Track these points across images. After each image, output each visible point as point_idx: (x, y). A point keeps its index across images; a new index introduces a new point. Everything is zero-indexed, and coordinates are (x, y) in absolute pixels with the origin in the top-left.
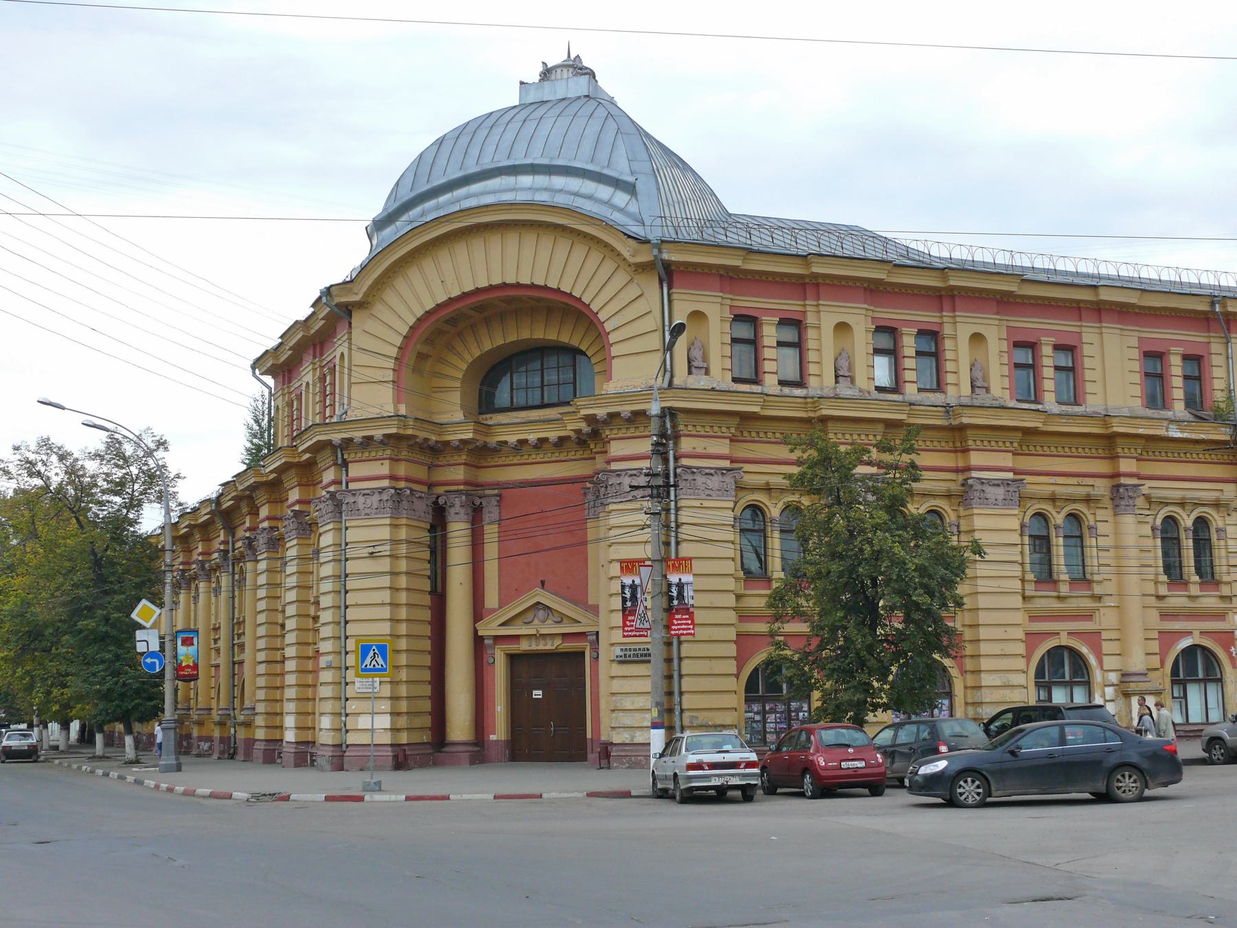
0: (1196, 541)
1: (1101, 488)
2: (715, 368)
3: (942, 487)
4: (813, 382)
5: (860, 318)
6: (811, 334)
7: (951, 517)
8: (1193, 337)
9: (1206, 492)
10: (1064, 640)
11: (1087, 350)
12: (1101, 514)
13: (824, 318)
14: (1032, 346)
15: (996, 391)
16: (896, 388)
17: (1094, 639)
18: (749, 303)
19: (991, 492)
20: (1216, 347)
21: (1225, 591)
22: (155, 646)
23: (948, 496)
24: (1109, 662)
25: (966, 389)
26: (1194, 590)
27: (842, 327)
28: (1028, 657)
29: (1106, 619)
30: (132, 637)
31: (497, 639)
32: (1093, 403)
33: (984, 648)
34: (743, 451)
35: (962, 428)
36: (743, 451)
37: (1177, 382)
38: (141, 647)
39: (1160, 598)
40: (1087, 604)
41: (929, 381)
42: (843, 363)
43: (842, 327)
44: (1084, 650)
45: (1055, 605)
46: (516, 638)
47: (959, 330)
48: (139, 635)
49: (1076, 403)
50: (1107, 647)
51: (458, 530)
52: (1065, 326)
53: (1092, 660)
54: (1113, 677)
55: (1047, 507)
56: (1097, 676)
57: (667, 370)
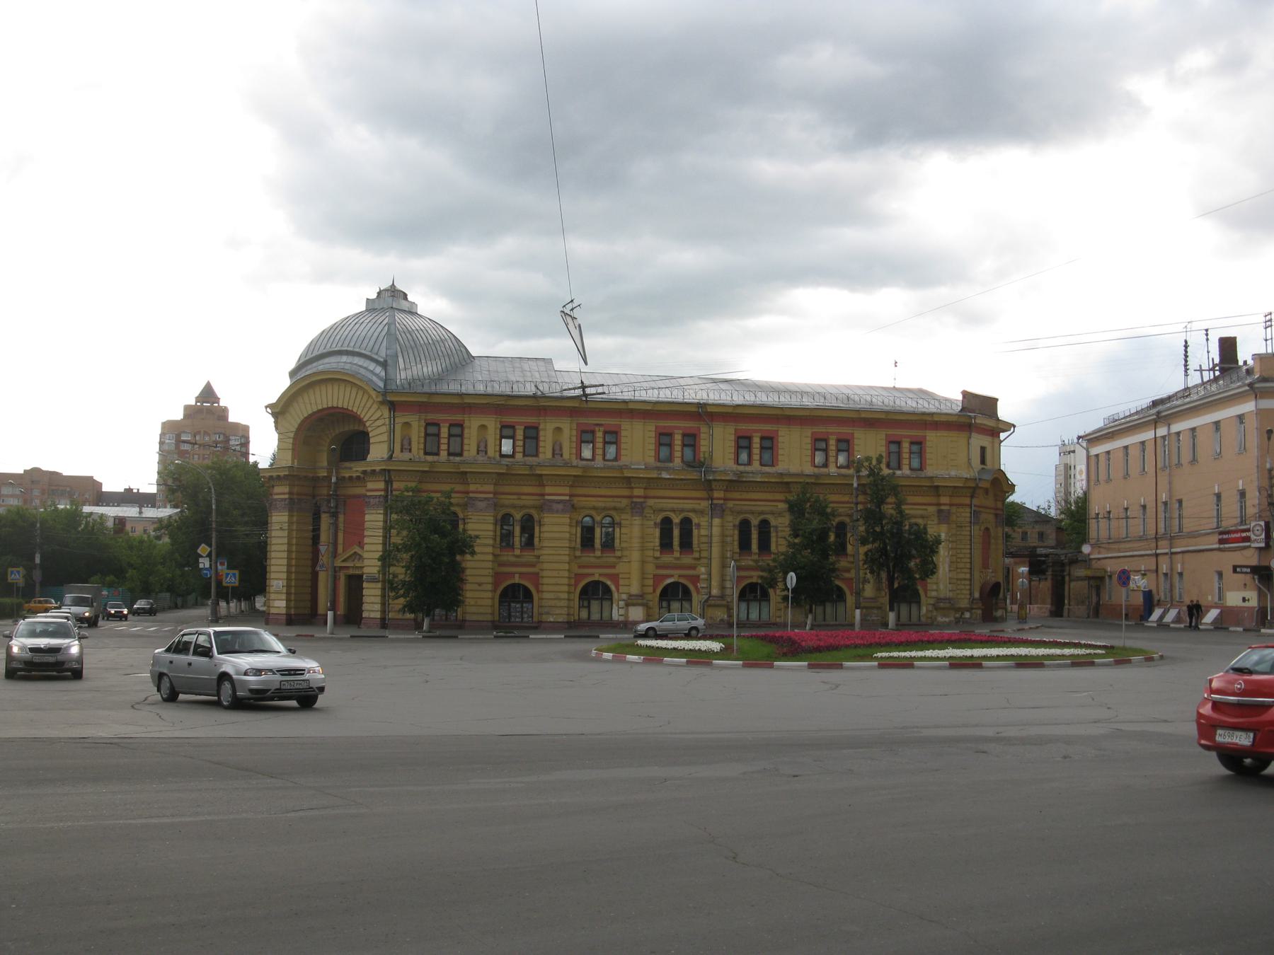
0: (760, 533)
1: (705, 504)
2: (414, 446)
3: (531, 503)
4: (465, 453)
5: (492, 424)
6: (466, 431)
7: (536, 517)
8: (689, 425)
9: (688, 505)
10: (517, 580)
11: (623, 433)
12: (623, 516)
13: (473, 425)
14: (899, 443)
15: (566, 456)
16: (593, 459)
17: (615, 578)
18: (432, 417)
19: (555, 506)
20: (704, 429)
21: (618, 554)
22: (207, 565)
23: (535, 507)
24: (622, 589)
25: (549, 455)
26: (517, 552)
27: (483, 427)
28: (576, 585)
29: (621, 568)
30: (198, 562)
31: (341, 568)
32: (930, 471)
33: (566, 581)
34: (729, 495)
35: (937, 487)
36: (729, 495)
37: (678, 448)
38: (201, 566)
39: (657, 558)
40: (533, 560)
41: (916, 464)
42: (557, 448)
43: (483, 427)
44: (609, 583)
45: (593, 560)
46: (347, 568)
47: (548, 429)
48: (201, 560)
49: (773, 465)
50: (621, 582)
51: (325, 520)
52: (610, 422)
53: (613, 588)
54: (624, 596)
55: (593, 513)
56: (615, 595)
57: (391, 451)
